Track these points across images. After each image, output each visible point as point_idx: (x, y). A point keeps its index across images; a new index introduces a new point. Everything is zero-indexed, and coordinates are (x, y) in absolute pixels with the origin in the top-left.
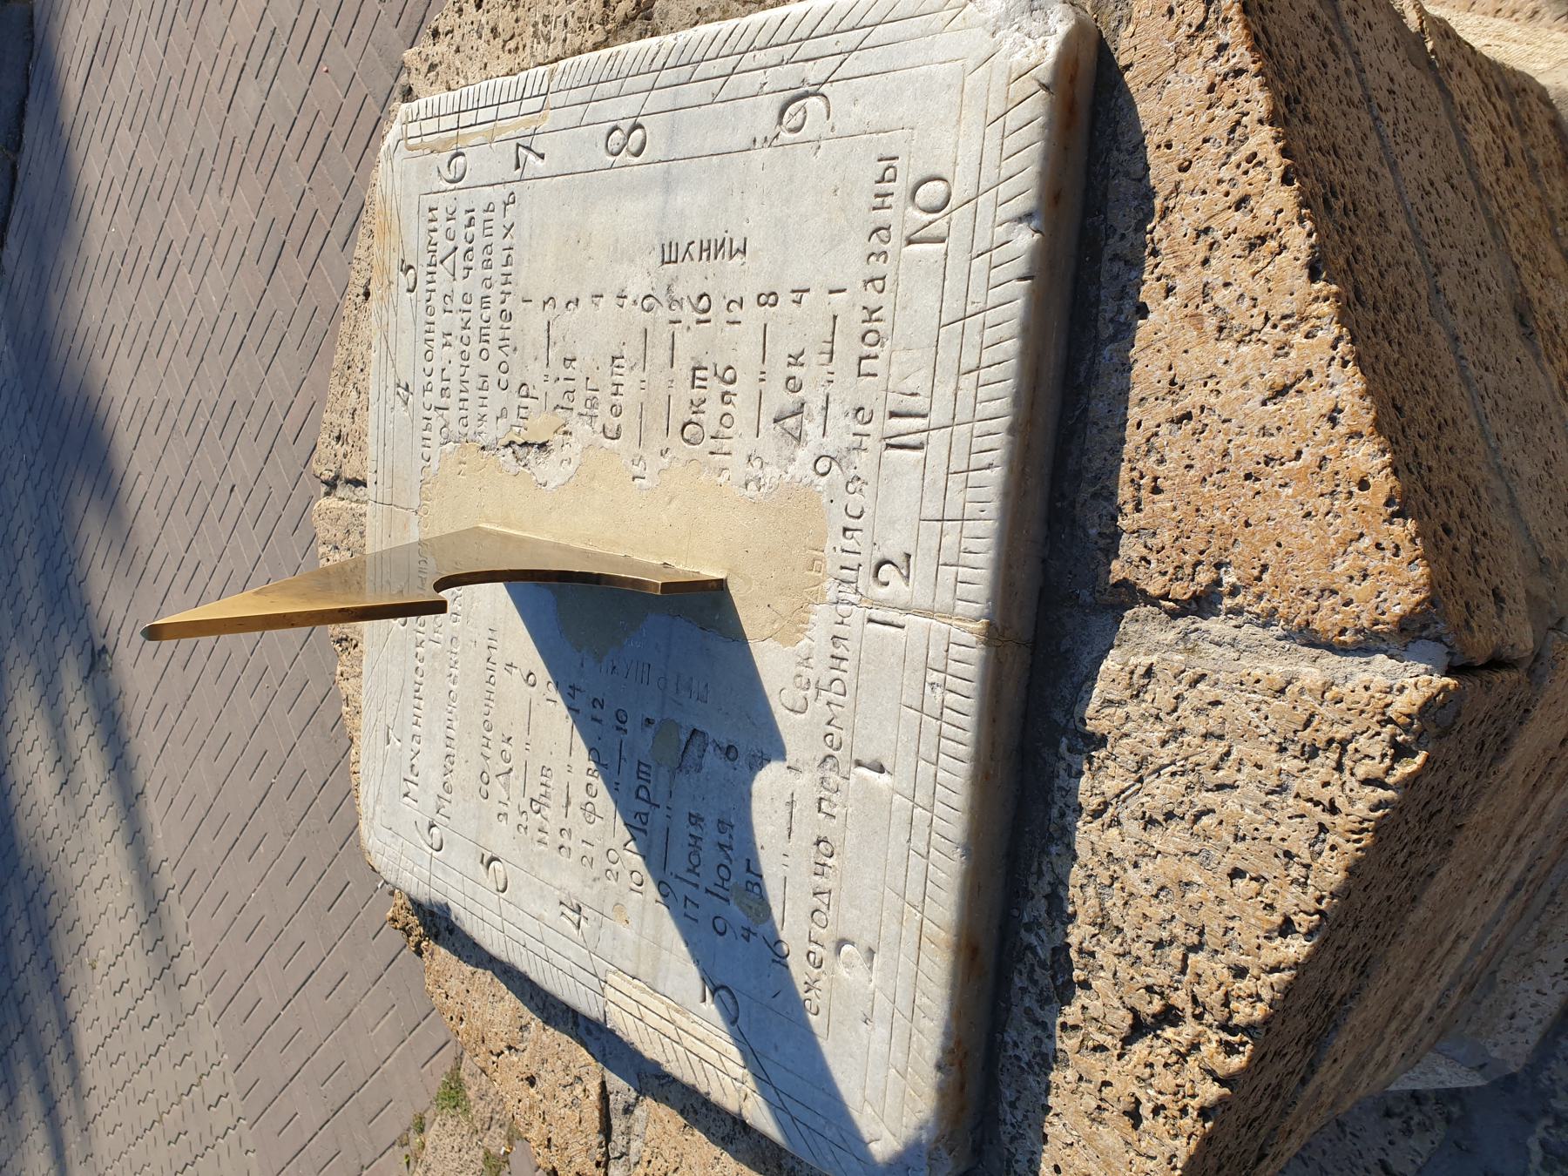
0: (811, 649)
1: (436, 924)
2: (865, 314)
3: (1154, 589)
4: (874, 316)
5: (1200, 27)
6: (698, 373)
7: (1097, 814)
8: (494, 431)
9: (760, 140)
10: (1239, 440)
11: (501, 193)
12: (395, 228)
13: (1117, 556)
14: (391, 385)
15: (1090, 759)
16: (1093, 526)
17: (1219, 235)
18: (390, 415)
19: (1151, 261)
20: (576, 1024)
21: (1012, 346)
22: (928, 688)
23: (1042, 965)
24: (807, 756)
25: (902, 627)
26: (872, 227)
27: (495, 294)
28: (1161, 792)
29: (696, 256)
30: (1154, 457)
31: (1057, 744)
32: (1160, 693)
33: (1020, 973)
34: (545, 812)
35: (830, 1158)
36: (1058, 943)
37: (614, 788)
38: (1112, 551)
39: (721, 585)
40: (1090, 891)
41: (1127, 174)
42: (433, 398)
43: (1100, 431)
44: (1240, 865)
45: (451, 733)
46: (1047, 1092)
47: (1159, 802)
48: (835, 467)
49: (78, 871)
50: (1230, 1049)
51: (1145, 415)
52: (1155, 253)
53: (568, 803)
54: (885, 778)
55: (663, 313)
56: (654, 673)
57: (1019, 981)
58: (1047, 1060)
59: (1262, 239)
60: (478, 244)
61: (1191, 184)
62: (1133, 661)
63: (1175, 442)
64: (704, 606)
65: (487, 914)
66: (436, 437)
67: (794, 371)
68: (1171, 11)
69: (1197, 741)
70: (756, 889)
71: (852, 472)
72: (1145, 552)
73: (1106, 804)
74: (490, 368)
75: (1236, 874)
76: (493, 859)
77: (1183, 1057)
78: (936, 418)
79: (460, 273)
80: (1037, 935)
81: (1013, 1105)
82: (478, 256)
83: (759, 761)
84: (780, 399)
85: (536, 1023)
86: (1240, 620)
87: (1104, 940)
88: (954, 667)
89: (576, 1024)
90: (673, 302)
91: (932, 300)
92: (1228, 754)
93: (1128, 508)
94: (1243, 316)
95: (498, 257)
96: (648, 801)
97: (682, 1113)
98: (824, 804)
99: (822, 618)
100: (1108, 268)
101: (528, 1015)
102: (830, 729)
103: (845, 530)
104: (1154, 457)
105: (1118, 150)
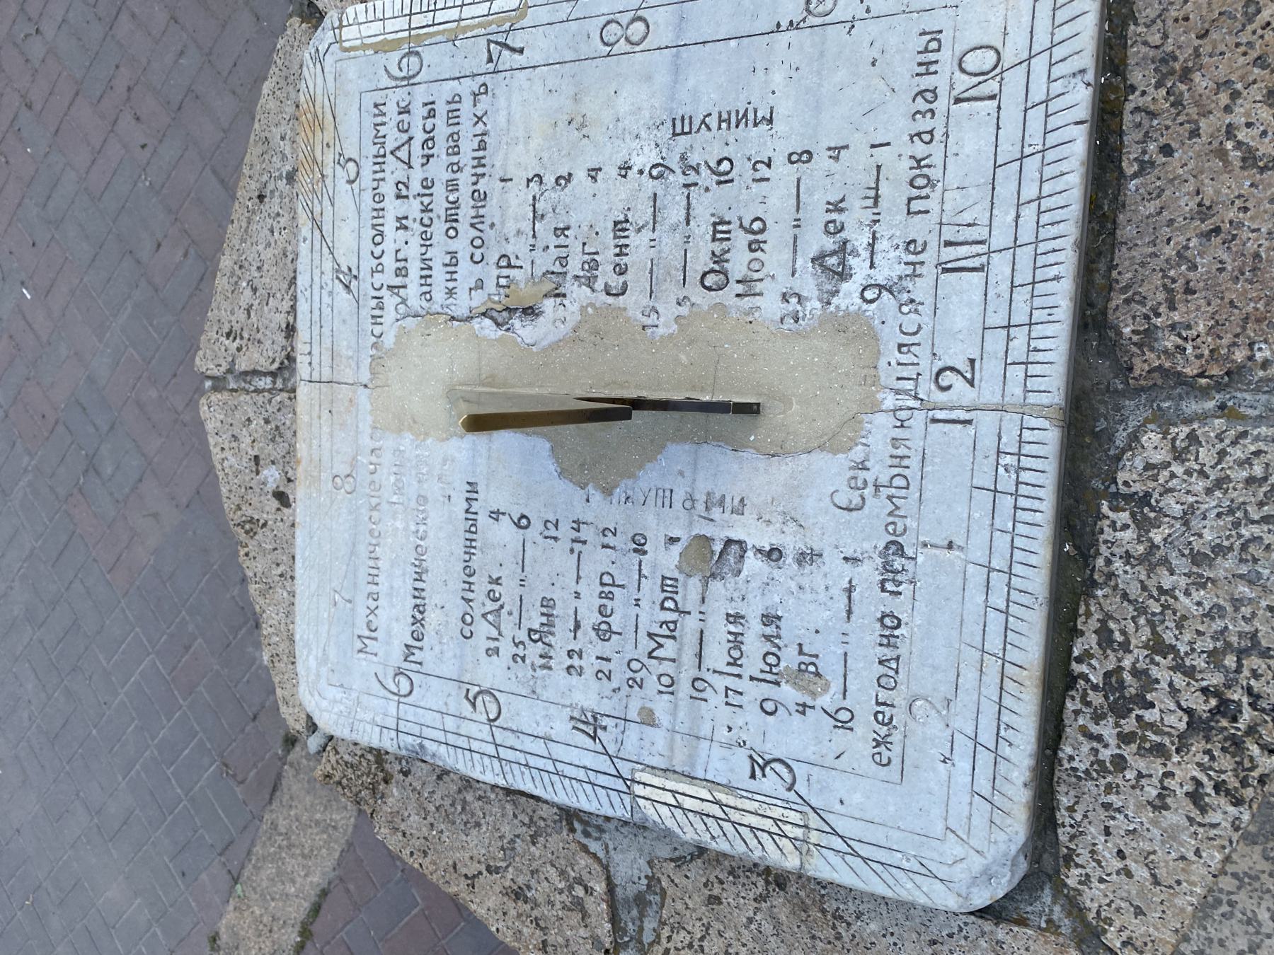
4: (923, 163)
6: (720, 228)
9: (784, 25)
11: (474, 85)
14: (328, 265)
16: (1127, 325)
17: (1239, 86)
22: (1001, 470)
23: (1095, 688)
26: (917, 90)
27: (465, 179)
31: (1099, 506)
33: (1073, 698)
35: (909, 885)
41: (1145, 43)
42: (389, 278)
43: (1129, 249)
48: (885, 293)
55: (677, 179)
57: (1070, 705)
60: (442, 131)
61: (1209, 49)
67: (834, 216)
71: (905, 297)
72: (1180, 341)
74: (461, 245)
78: (996, 243)
79: (417, 161)
80: (1090, 665)
81: (1071, 809)
84: (816, 241)
95: (468, 146)
96: (677, 610)
103: (900, 346)
105: (1136, 24)
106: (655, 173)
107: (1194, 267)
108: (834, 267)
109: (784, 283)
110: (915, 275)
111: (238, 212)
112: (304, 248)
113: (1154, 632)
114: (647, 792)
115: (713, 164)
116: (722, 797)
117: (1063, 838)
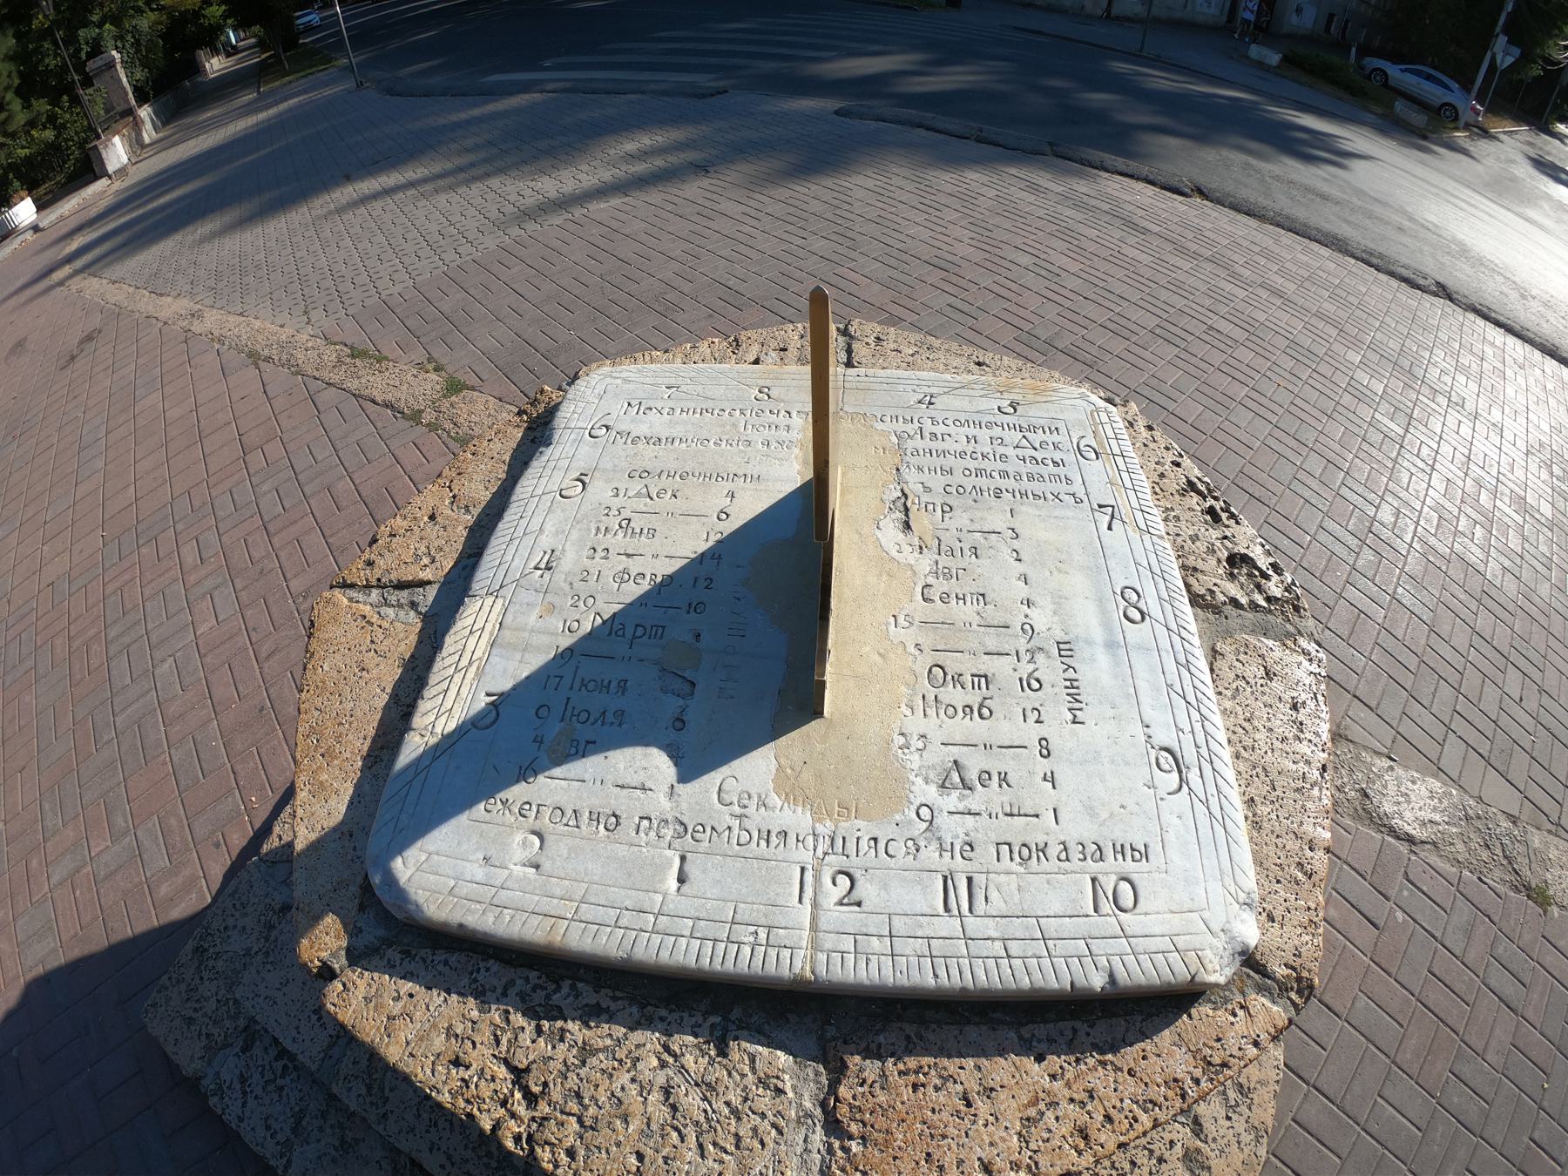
0: (773, 809)
1: (538, 431)
2: (1041, 846)
3: (843, 1091)
5: (1209, 1063)
7: (666, 1048)
8: (913, 480)
10: (954, 1147)
11: (1081, 494)
12: (1039, 398)
13: (864, 1059)
14: (934, 390)
15: (708, 1042)
17: (1089, 1107)
18: (909, 388)
19: (1073, 1059)
20: (470, 556)
21: (1025, 983)
22: (752, 929)
23: (548, 997)
24: (684, 806)
25: (800, 901)
28: (692, 1101)
29: (1067, 675)
30: (938, 1082)
32: (764, 1101)
34: (621, 534)
36: (566, 1012)
37: (642, 601)
38: (867, 1054)
39: (819, 713)
40: (608, 1042)
41: (1127, 1030)
44: (646, 1159)
45: (677, 442)
46: (460, 994)
47: (684, 1100)
48: (925, 825)
49: (585, 167)
50: (517, 1138)
51: (966, 1071)
52: (1078, 1061)
53: (628, 556)
54: (673, 884)
55: (1022, 644)
56: (736, 643)
57: (533, 975)
58: (482, 996)
59: (1086, 1138)
60: (1041, 469)
61: (1121, 1080)
62: (787, 1077)
63: (949, 1098)
64: (796, 697)
65: (544, 481)
66: (900, 427)
67: (995, 778)
68: (1219, 1040)
69: (733, 1130)
70: (573, 751)
71: (922, 844)
73: (675, 1056)
74: (958, 478)
75: (640, 1157)
76: (584, 484)
77: (504, 1103)
79: (1020, 452)
81: (446, 963)
82: (1035, 469)
83: (676, 756)
84: (974, 764)
85: (469, 519)
86: (823, 1152)
87: (575, 1051)
88: (773, 953)
89: (470, 556)
90: (1032, 652)
91: (1056, 908)
92: (726, 1152)
93: (901, 1066)
94: (1037, 1133)
95: (1037, 487)
96: (634, 637)
97: (412, 656)
98: (645, 823)
99: (798, 819)
100: (1066, 1025)
101: (476, 512)
102: (708, 830)
103: (875, 840)
104: (938, 1082)
106: (1027, 627)
107: (937, 1089)
108: (954, 777)
109: (936, 736)
110: (942, 849)
111: (967, 350)
112: (948, 377)
113: (598, 1050)
114: (486, 609)
115: (1036, 674)
116: (473, 669)
117: (423, 953)
